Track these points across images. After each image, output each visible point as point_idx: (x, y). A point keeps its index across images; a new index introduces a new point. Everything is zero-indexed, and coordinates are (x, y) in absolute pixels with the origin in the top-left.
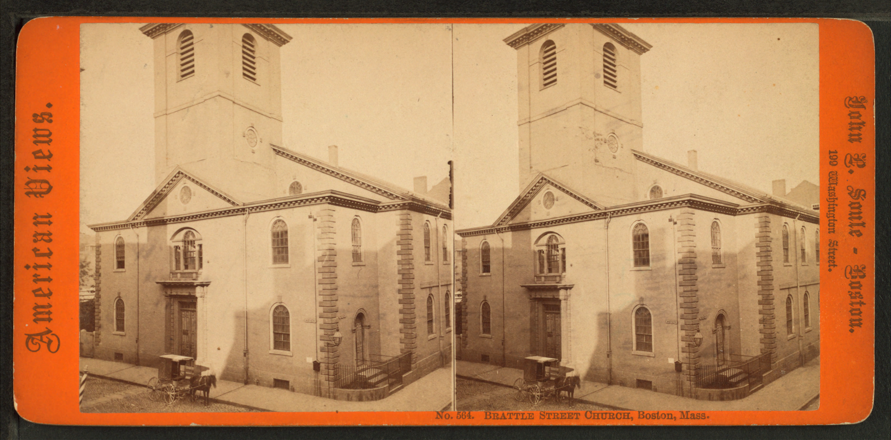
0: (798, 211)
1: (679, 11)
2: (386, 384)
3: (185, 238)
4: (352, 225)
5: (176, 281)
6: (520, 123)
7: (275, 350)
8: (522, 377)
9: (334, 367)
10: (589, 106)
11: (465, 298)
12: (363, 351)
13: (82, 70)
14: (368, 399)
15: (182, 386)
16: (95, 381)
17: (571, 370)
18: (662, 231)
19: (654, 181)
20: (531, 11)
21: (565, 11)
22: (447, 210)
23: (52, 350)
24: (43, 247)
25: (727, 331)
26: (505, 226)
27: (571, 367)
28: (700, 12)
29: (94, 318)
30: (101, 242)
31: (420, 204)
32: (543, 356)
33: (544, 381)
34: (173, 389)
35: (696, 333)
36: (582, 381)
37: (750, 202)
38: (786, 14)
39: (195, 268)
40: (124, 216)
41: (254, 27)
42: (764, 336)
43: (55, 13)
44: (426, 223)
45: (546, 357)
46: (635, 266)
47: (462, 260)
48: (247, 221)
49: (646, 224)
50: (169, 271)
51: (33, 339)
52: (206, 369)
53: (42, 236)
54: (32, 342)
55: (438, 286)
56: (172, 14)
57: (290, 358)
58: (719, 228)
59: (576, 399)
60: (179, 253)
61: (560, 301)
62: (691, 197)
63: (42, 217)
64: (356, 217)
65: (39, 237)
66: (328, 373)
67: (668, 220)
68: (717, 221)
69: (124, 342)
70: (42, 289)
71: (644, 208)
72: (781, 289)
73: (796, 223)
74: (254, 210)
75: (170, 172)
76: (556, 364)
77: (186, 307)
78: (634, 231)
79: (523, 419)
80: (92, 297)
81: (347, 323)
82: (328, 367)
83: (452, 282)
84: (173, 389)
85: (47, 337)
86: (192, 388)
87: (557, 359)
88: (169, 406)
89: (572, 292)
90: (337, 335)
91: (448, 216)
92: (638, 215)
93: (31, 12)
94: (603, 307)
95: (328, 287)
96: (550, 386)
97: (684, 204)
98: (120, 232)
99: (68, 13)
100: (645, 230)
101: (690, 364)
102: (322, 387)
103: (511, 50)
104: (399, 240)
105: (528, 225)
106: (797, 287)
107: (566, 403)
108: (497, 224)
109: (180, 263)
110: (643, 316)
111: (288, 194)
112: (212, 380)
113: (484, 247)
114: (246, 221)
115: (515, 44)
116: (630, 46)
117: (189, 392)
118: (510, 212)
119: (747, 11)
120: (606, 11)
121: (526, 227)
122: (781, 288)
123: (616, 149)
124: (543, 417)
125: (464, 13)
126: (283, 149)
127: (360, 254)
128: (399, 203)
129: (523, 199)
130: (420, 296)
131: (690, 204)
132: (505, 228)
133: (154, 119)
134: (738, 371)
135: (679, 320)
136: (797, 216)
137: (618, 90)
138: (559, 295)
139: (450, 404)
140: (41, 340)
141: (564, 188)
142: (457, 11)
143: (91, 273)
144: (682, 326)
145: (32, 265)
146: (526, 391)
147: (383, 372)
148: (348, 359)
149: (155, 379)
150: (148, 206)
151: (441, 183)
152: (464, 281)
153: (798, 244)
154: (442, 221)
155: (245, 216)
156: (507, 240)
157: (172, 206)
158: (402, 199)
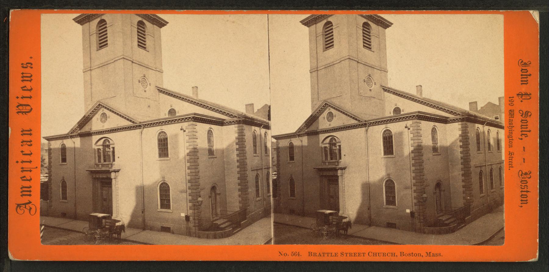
0: (263, 123)
1: (415, 6)
2: (230, 228)
6: (311, 71)
7: (161, 209)
12: (216, 209)
14: (220, 238)
17: (346, 218)
18: (176, 136)
24: (26, 149)
25: (442, 193)
27: (118, 219)
29: (48, 192)
30: (51, 147)
31: (250, 120)
33: (101, 228)
34: (98, 234)
36: (126, 228)
37: (232, 118)
39: (336, 159)
40: (66, 131)
41: (370, 18)
42: (242, 199)
44: (254, 132)
46: (159, 158)
48: (143, 132)
50: (94, 164)
51: (20, 207)
52: (119, 221)
53: (26, 143)
54: (20, 208)
55: (262, 169)
57: (170, 214)
58: (212, 133)
59: (122, 239)
60: (327, 150)
62: (419, 113)
63: (26, 131)
64: (210, 129)
65: (25, 143)
66: (195, 222)
67: (404, 127)
68: (435, 127)
73: (261, 130)
74: (146, 126)
75: (319, 104)
76: (109, 218)
78: (384, 134)
80: (46, 180)
81: (205, 192)
84: (98, 234)
85: (29, 206)
90: (200, 199)
91: (267, 127)
92: (386, 125)
93: (19, 7)
94: (365, 180)
95: (193, 171)
96: (106, 231)
98: (63, 141)
100: (390, 133)
101: (195, 216)
102: (191, 231)
104: (237, 142)
105: (90, 133)
108: (71, 132)
109: (101, 158)
110: (164, 189)
111: (167, 116)
112: (122, 227)
113: (62, 147)
114: (367, 131)
115: (307, 24)
116: (154, 23)
117: (108, 235)
118: (79, 125)
119: (457, 6)
120: (370, 6)
121: (89, 134)
122: (252, 169)
123: (146, 86)
127: (437, 148)
130: (251, 176)
131: (194, 119)
133: (83, 73)
134: (225, 220)
135: (188, 190)
136: (261, 126)
137: (373, 50)
138: (337, 173)
139: (271, 239)
140: (25, 207)
141: (339, 109)
142: (279, 6)
143: (45, 166)
144: (189, 194)
148: (207, 213)
150: (80, 125)
154: (263, 131)
155: (141, 130)
156: (77, 142)
157: (96, 124)
158: (239, 117)
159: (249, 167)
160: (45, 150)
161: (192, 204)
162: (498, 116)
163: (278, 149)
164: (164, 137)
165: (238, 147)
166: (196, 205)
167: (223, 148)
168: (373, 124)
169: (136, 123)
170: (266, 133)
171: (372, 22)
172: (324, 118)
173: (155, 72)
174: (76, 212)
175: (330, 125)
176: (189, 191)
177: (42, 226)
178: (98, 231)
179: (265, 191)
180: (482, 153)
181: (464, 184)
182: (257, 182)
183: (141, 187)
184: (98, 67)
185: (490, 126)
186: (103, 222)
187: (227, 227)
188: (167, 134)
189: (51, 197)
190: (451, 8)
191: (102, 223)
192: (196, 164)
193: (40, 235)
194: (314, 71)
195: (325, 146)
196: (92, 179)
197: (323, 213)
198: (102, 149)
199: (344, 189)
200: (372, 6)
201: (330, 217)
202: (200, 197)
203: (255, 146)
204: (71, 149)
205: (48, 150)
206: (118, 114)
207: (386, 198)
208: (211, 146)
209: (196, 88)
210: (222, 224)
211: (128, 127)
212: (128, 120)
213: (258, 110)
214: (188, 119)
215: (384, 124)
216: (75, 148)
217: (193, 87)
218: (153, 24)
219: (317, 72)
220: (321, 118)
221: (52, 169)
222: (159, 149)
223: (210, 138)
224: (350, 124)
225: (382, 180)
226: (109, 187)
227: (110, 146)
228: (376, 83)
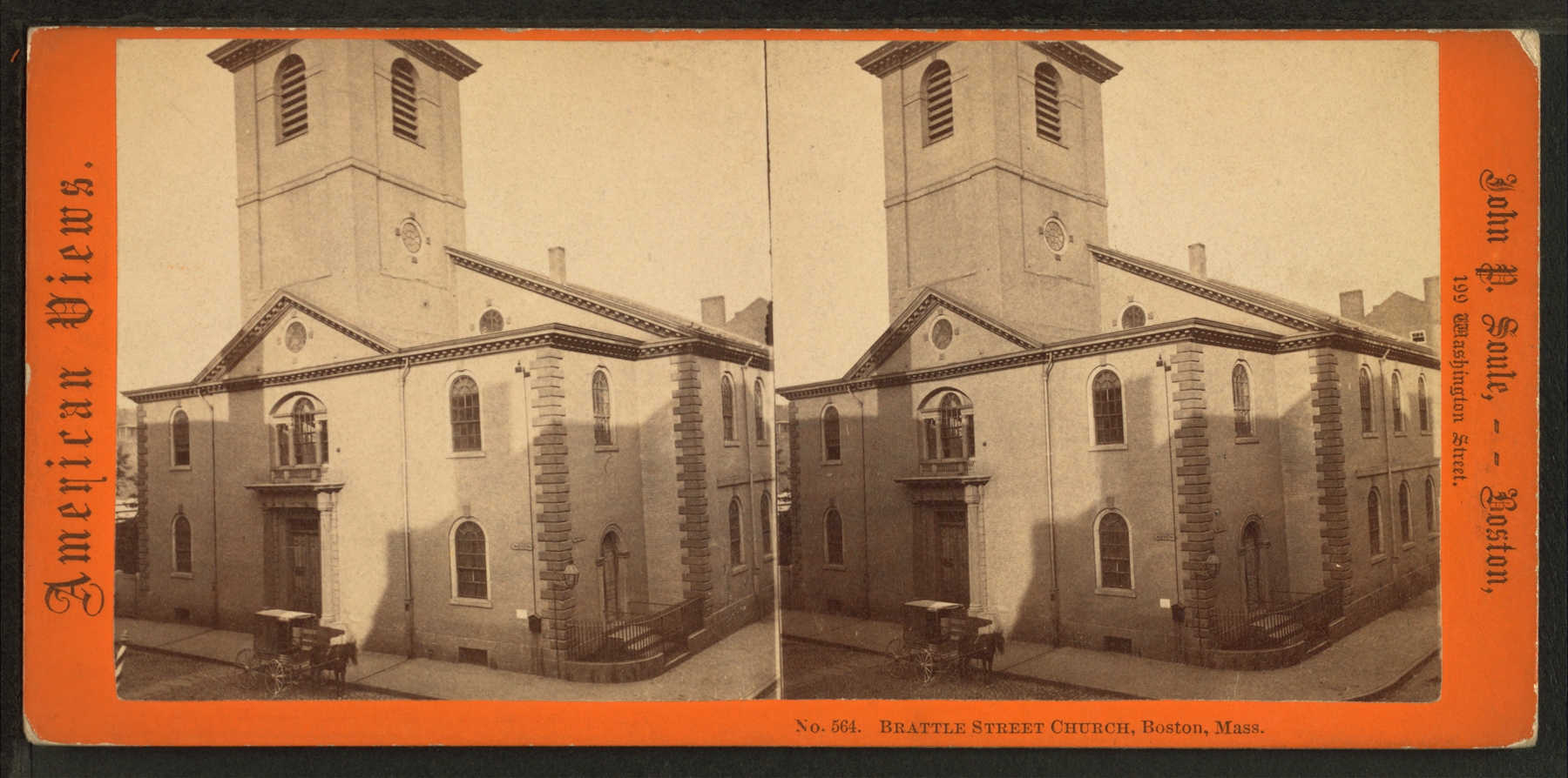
0: (750, 351)
1: (1185, 18)
2: (658, 653)
5: (930, 478)
7: (461, 599)
9: (565, 626)
12: (616, 598)
18: (503, 388)
21: (984, 16)
24: (76, 427)
25: (1263, 552)
26: (217, 383)
27: (338, 627)
29: (137, 549)
30: (147, 420)
33: (291, 653)
34: (280, 669)
36: (360, 652)
37: (663, 337)
38: (1372, 22)
39: (961, 456)
40: (187, 373)
41: (1056, 50)
43: (94, 20)
44: (725, 376)
45: (294, 610)
46: (455, 451)
49: (1116, 372)
50: (269, 468)
51: (58, 591)
52: (339, 633)
55: (748, 483)
56: (299, 22)
57: (486, 612)
58: (606, 382)
59: (349, 684)
60: (934, 430)
61: (966, 505)
62: (1195, 323)
64: (599, 369)
65: (70, 409)
67: (514, 370)
68: (1243, 363)
70: (74, 505)
71: (471, 349)
75: (910, 297)
76: (312, 622)
78: (1096, 382)
80: (133, 515)
81: (586, 550)
82: (555, 624)
83: (774, 476)
84: (280, 669)
87: (314, 615)
90: (570, 569)
91: (764, 363)
93: (53, 19)
94: (1043, 515)
95: (553, 488)
96: (302, 660)
99: (117, 20)
100: (1114, 381)
104: (678, 405)
106: (748, 483)
108: (201, 379)
109: (287, 453)
110: (470, 539)
111: (477, 332)
112: (349, 650)
113: (177, 419)
115: (878, 69)
116: (441, 65)
117: (308, 673)
118: (225, 359)
119: (1304, 17)
120: (1057, 17)
121: (254, 384)
122: (721, 484)
123: (417, 247)
127: (1249, 423)
128: (1313, 336)
129: (896, 332)
130: (716, 503)
131: (554, 341)
132: (866, 382)
133: (884, 210)
134: (644, 630)
139: (774, 685)
141: (969, 312)
142: (797, 17)
143: (130, 473)
145: (56, 460)
148: (590, 610)
153: (1390, 406)
154: (751, 374)
155: (402, 371)
156: (220, 407)
157: (274, 356)
158: (682, 335)
159: (711, 479)
160: (129, 428)
161: (548, 585)
162: (1423, 331)
163: (793, 427)
164: (467, 392)
165: (679, 422)
166: (559, 588)
167: (638, 424)
168: (1064, 354)
170: (759, 381)
171: (1063, 62)
172: (926, 338)
176: (540, 547)
178: (929, 651)
179: (757, 547)
180: (738, 446)
181: (1324, 525)
182: (734, 521)
185: (1400, 361)
186: (294, 635)
187: (648, 648)
188: (478, 384)
189: (147, 565)
191: (291, 637)
192: (559, 470)
194: (898, 202)
195: (930, 417)
198: (290, 428)
199: (982, 540)
201: (944, 622)
202: (571, 562)
203: (728, 417)
204: (202, 425)
206: (336, 327)
207: (1103, 568)
210: (634, 641)
211: (367, 364)
214: (537, 342)
216: (862, 417)
217: (550, 250)
218: (438, 68)
219: (906, 206)
220: (916, 338)
222: (455, 426)
225: (1089, 515)
227: (313, 419)
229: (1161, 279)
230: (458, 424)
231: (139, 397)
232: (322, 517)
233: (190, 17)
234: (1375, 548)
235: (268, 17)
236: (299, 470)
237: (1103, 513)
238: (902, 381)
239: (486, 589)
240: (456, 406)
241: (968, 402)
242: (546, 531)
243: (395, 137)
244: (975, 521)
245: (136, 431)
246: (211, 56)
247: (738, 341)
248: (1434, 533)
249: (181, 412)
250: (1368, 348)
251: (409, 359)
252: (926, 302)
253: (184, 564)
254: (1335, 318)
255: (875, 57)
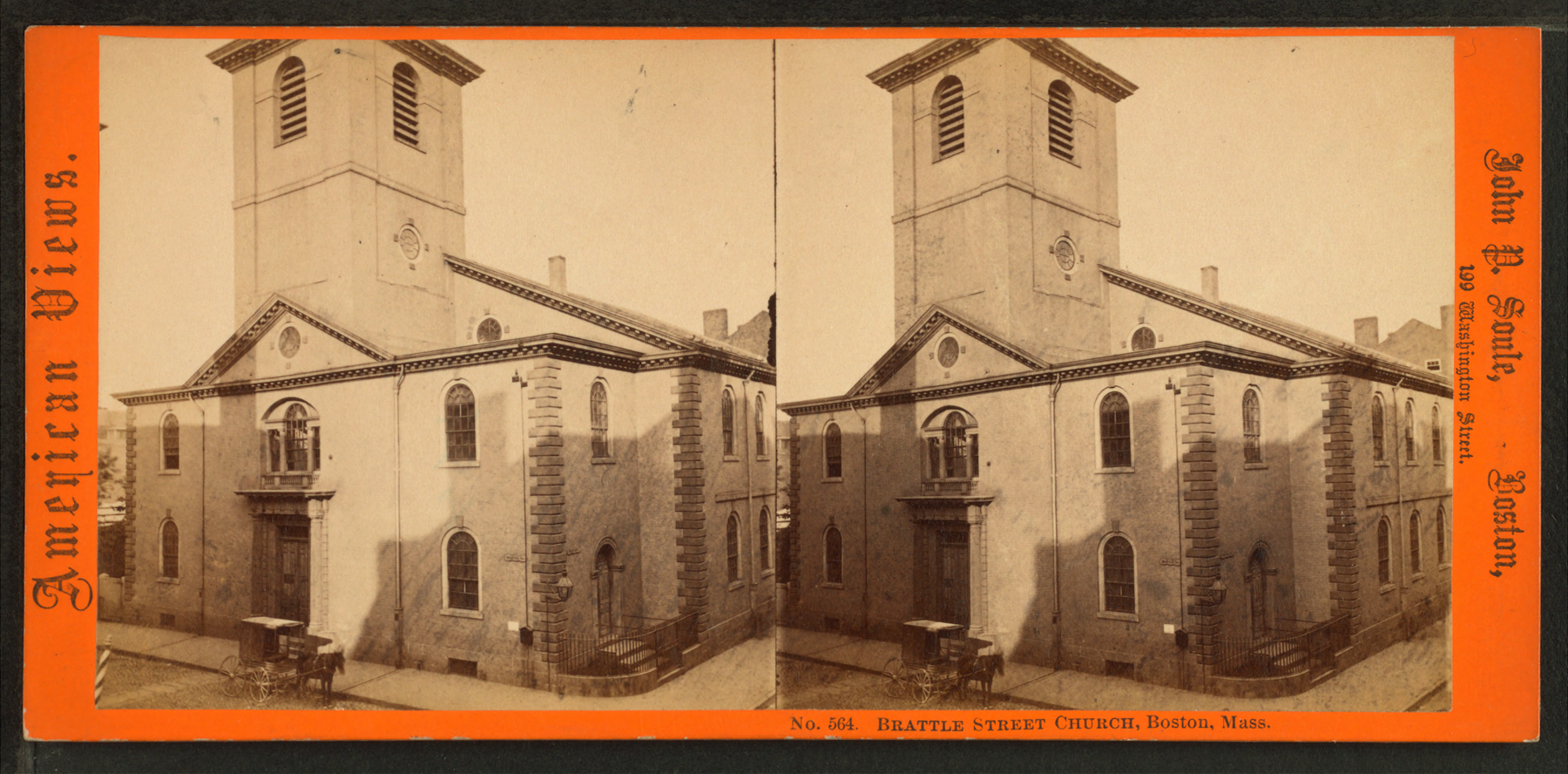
0: (752, 365)
2: (651, 667)
3: (947, 425)
4: (592, 393)
8: (236, 652)
10: (1021, 190)
11: (795, 519)
13: (103, 127)
15: (942, 672)
16: (125, 662)
18: (499, 398)
19: (485, 310)
20: (936, 15)
21: (993, 15)
22: (1413, 374)
23: (78, 607)
25: (616, 576)
28: (1232, 17)
29: (124, 553)
30: (136, 424)
31: (714, 356)
32: (937, 620)
33: (276, 661)
34: (265, 676)
35: (1213, 581)
38: (1385, 19)
40: (841, 387)
44: (726, 390)
46: (1104, 467)
47: (791, 456)
48: (402, 385)
55: (747, 498)
60: (937, 450)
62: (554, 338)
64: (598, 380)
67: (1164, 387)
68: (602, 381)
69: (180, 593)
72: (717, 502)
74: (413, 368)
75: (263, 302)
76: (299, 631)
77: (296, 536)
78: (1103, 404)
79: (944, 730)
80: (120, 518)
84: (265, 676)
86: (960, 676)
87: (302, 623)
88: (258, 705)
89: (992, 512)
91: (770, 379)
92: (1110, 378)
96: (290, 669)
97: (1194, 358)
98: (832, 416)
100: (1122, 403)
102: (535, 672)
103: (224, 74)
107: (978, 701)
110: (462, 551)
111: (475, 341)
112: (336, 660)
113: (167, 423)
114: (1055, 395)
115: (229, 64)
117: (956, 683)
118: (218, 362)
120: (1066, 16)
121: (245, 389)
122: (719, 499)
123: (415, 253)
124: (1262, 722)
125: (817, 20)
126: (1121, 273)
128: (676, 355)
129: (241, 339)
130: (714, 516)
132: (869, 399)
133: (232, 211)
136: (749, 373)
137: (1077, 163)
141: (976, 331)
143: (117, 476)
146: (242, 678)
147: (648, 647)
149: (233, 659)
151: (754, 320)
152: (794, 491)
153: (751, 424)
154: (753, 388)
157: (267, 361)
160: (118, 430)
161: (541, 597)
162: (1439, 360)
163: (795, 444)
164: (464, 401)
166: (553, 597)
167: (636, 438)
168: (1072, 375)
169: (1041, 368)
170: (761, 395)
171: (1079, 81)
172: (931, 356)
173: (442, 211)
174: (202, 615)
175: (288, 366)
176: (534, 559)
177: (103, 650)
178: (928, 671)
179: (756, 562)
180: (737, 461)
182: (732, 535)
183: (395, 543)
184: (934, 208)
185: (1415, 389)
186: (281, 643)
190: (1301, 19)
191: (939, 648)
193: (94, 679)
194: (908, 218)
196: (254, 517)
197: (924, 629)
198: (282, 433)
199: (983, 560)
200: (1072, 16)
201: (943, 642)
204: (855, 438)
205: (789, 442)
207: (1107, 592)
208: (1254, 436)
209: (559, 260)
211: (361, 370)
212: (360, 348)
213: (1391, 335)
214: (535, 352)
215: (452, 367)
216: (865, 435)
217: (551, 259)
218: (1094, 90)
220: (922, 355)
221: (138, 486)
222: (450, 435)
223: (1250, 415)
224: (1007, 375)
225: (1096, 536)
226: (958, 547)
227: (305, 425)
228: (1085, 259)
229: (527, 295)
230: (1108, 439)
231: (792, 409)
232: (312, 525)
233: (192, 19)
234: (1384, 577)
235: (271, 18)
236: (290, 476)
237: (1109, 536)
238: (908, 398)
239: (478, 600)
240: (451, 415)
241: (972, 422)
242: (540, 543)
243: (1050, 157)
244: (977, 541)
245: (124, 434)
246: (211, 56)
247: (1389, 361)
248: (1444, 564)
249: (834, 425)
250: (728, 368)
251: (404, 366)
252: (933, 320)
253: (835, 572)
254: (1348, 345)
255: (224, 52)
